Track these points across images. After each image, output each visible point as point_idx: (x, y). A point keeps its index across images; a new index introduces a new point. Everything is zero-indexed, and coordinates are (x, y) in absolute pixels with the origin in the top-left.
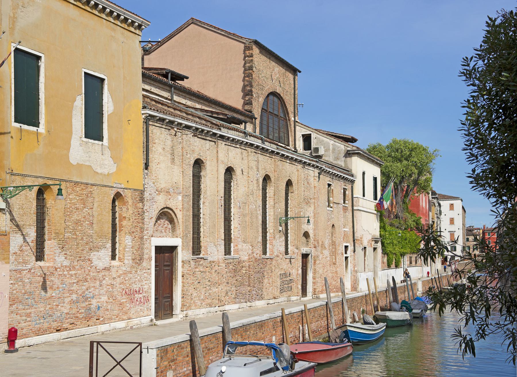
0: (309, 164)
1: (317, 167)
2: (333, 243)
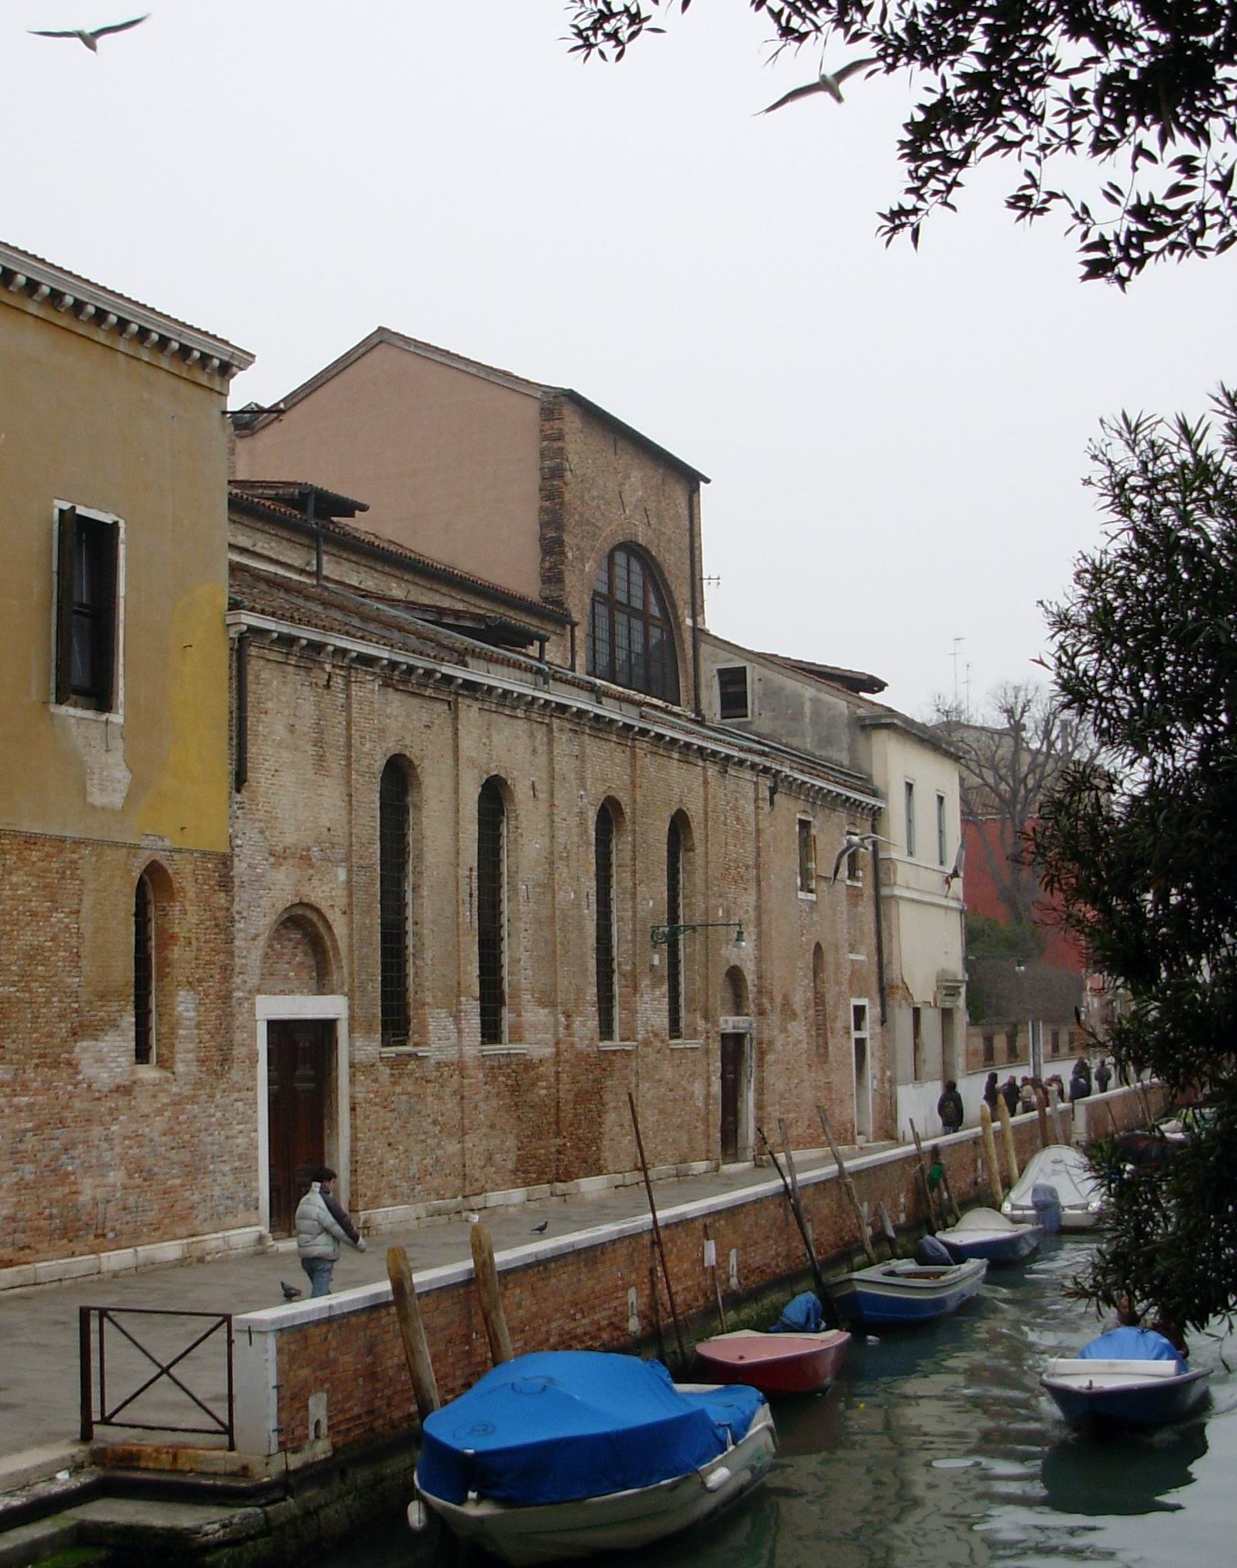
0: (741, 762)
1: (766, 770)
2: (819, 999)
